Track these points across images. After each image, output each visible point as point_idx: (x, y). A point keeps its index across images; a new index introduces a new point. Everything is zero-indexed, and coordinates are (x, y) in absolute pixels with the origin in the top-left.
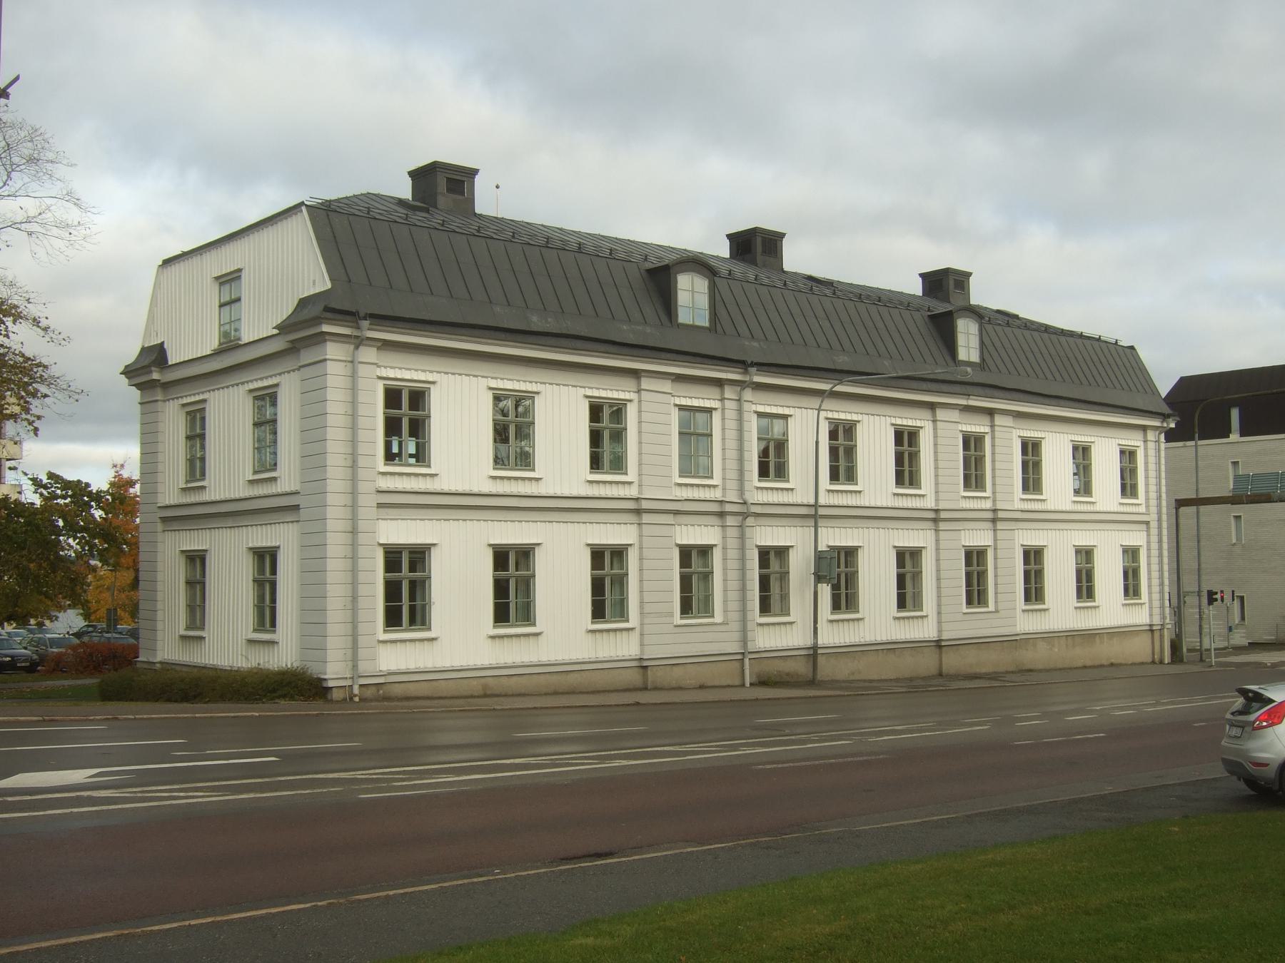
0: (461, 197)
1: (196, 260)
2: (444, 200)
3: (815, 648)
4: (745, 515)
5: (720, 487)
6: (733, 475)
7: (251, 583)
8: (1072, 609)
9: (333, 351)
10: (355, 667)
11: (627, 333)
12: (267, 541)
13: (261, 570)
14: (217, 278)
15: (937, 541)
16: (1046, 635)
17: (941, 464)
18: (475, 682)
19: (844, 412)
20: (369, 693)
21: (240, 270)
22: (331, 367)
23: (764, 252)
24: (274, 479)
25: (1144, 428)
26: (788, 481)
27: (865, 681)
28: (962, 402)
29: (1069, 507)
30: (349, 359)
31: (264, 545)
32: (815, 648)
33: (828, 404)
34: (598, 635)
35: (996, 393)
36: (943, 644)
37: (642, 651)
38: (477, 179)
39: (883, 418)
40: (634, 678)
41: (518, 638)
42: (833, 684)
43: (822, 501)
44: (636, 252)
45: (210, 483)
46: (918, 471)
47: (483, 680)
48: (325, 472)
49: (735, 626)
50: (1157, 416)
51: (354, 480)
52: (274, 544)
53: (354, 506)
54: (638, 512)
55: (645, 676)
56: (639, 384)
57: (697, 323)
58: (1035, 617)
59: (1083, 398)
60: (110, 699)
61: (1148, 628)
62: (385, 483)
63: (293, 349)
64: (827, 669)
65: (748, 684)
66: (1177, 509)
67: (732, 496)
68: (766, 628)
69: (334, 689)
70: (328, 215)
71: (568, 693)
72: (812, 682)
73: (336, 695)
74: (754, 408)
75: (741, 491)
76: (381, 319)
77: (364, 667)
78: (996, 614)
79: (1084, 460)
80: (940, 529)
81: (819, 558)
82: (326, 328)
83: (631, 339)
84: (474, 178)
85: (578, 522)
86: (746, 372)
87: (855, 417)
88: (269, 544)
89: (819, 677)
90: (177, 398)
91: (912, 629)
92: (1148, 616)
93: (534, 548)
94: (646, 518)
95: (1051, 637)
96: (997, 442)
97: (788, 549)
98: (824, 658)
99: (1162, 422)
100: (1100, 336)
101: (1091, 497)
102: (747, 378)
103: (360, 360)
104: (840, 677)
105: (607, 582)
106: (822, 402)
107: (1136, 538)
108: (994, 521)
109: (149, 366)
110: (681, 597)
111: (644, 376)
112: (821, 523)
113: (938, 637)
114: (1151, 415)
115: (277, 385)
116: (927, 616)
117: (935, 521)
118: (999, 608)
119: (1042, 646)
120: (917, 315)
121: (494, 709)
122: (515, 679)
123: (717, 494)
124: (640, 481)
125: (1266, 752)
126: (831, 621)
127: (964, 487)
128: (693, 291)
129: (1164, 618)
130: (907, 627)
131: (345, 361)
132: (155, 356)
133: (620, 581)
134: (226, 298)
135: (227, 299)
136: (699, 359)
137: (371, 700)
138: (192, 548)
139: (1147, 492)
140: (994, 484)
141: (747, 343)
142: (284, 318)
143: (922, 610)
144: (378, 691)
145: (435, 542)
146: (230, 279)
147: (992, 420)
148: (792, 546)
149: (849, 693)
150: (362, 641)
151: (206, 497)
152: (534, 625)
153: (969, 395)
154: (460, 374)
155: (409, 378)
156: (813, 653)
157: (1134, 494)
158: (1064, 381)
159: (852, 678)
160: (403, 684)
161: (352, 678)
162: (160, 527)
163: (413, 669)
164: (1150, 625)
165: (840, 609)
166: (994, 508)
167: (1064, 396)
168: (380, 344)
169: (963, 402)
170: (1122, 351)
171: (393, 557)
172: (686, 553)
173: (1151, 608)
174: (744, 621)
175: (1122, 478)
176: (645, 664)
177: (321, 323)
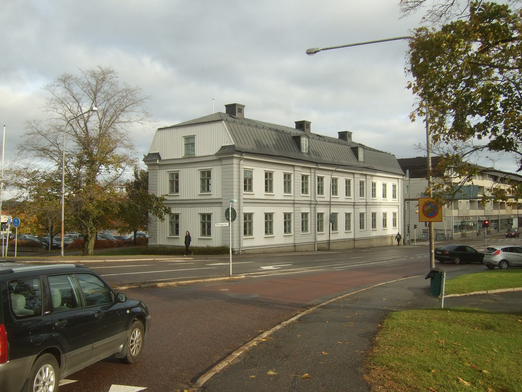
3: (329, 240)
4: (316, 204)
8: (344, 232)
9: (235, 161)
10: (240, 245)
12: (207, 211)
16: (301, 244)
18: (262, 250)
25: (398, 179)
26: (323, 195)
29: (391, 201)
32: (329, 240)
36: (356, 239)
37: (294, 241)
40: (292, 248)
42: (332, 250)
43: (331, 201)
49: (313, 235)
52: (251, 212)
55: (295, 248)
56: (294, 169)
64: (333, 246)
66: (405, 202)
67: (313, 199)
72: (329, 250)
75: (315, 198)
82: (235, 155)
86: (317, 165)
89: (330, 249)
94: (296, 205)
101: (323, 195)
102: (317, 167)
107: (396, 210)
112: (331, 206)
119: (375, 240)
123: (309, 199)
139: (398, 197)
140: (366, 195)
151: (180, 198)
156: (329, 242)
173: (399, 229)
174: (239, 237)
175: (346, 190)
176: (296, 245)
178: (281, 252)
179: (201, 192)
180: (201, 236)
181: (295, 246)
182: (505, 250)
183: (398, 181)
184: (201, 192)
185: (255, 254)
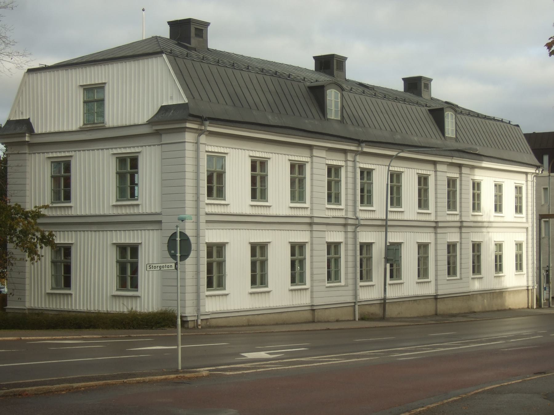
3: (385, 299)
4: (357, 226)
7: (115, 263)
8: (514, 275)
9: (189, 137)
17: (439, 196)
18: (244, 318)
23: (337, 69)
24: (138, 205)
29: (249, 211)
30: (195, 142)
32: (385, 299)
36: (439, 297)
37: (312, 301)
38: (432, 83)
39: (413, 170)
40: (308, 316)
41: (215, 297)
44: (177, 50)
47: (248, 317)
48: (185, 203)
49: (351, 287)
50: (534, 167)
55: (313, 315)
56: (312, 153)
58: (394, 287)
59: (348, 136)
62: (209, 210)
64: (391, 311)
65: (357, 319)
67: (350, 215)
69: (189, 322)
70: (175, 59)
71: (281, 324)
72: (383, 318)
75: (355, 212)
76: (215, 120)
77: (202, 310)
80: (438, 232)
81: (388, 249)
84: (207, 28)
85: (253, 230)
86: (359, 145)
87: (401, 170)
92: (526, 282)
93: (267, 244)
94: (315, 227)
97: (340, 244)
100: (502, 119)
102: (360, 149)
106: (391, 162)
113: (435, 293)
114: (531, 166)
116: (430, 282)
118: (463, 277)
120: (423, 109)
121: (273, 332)
122: (260, 316)
127: (418, 207)
130: (424, 286)
131: (193, 143)
136: (340, 139)
139: (527, 210)
141: (357, 129)
143: (428, 278)
144: (207, 323)
145: (270, 241)
147: (461, 170)
149: (413, 324)
153: (453, 157)
156: (384, 303)
158: (514, 151)
159: (398, 316)
163: (226, 310)
166: (461, 220)
167: (494, 156)
168: (327, 149)
169: (449, 160)
170: (513, 128)
173: (528, 277)
176: (315, 308)
178: (284, 323)
179: (117, 200)
180: (117, 290)
181: (313, 310)
184: (117, 200)
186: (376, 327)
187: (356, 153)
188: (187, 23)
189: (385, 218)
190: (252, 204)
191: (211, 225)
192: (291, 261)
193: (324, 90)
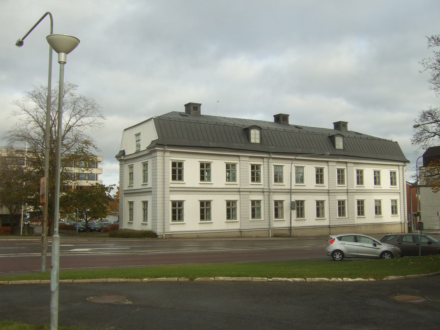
0: (197, 111)
1: (131, 130)
2: (192, 112)
3: (291, 227)
4: (270, 192)
5: (263, 185)
6: (267, 181)
7: (142, 210)
9: (159, 154)
10: (164, 230)
11: (236, 146)
13: (145, 207)
14: (135, 135)
15: (329, 198)
18: (195, 234)
19: (300, 164)
20: (167, 236)
21: (140, 133)
22: (158, 158)
23: (283, 120)
24: (147, 184)
26: (283, 183)
27: (304, 236)
28: (336, 160)
30: (163, 156)
31: (145, 200)
32: (291, 227)
33: (294, 162)
34: (228, 223)
35: (347, 157)
36: (331, 226)
38: (348, 124)
40: (238, 234)
41: (206, 224)
42: (296, 237)
45: (134, 185)
46: (323, 179)
49: (267, 221)
51: (164, 185)
52: (147, 200)
53: (164, 191)
54: (239, 192)
56: (328, 164)
57: (256, 142)
59: (376, 158)
60: (111, 237)
61: (400, 223)
63: (150, 153)
64: (294, 233)
68: (276, 222)
72: (290, 236)
73: (159, 237)
74: (273, 164)
75: (269, 186)
77: (166, 230)
78: (348, 218)
79: (378, 175)
82: (157, 148)
83: (237, 147)
86: (270, 155)
88: (146, 200)
90: (127, 164)
91: (396, 219)
94: (241, 193)
95: (366, 225)
96: (348, 171)
98: (294, 230)
99: (404, 164)
103: (165, 156)
104: (299, 235)
105: (256, 209)
106: (292, 162)
107: (396, 197)
108: (347, 193)
109: (121, 156)
110: (252, 214)
111: (241, 157)
112: (292, 194)
115: (147, 161)
117: (328, 193)
124: (240, 184)
125: (329, 249)
126: (296, 220)
128: (255, 134)
129: (405, 220)
132: (123, 153)
133: (235, 209)
134: (137, 140)
135: (138, 140)
137: (168, 238)
138: (130, 201)
142: (149, 145)
144: (170, 236)
146: (138, 135)
148: (284, 200)
150: (166, 224)
151: (133, 188)
152: (211, 220)
154: (189, 158)
155: (178, 159)
156: (290, 229)
157: (395, 184)
159: (302, 235)
160: (176, 235)
161: (163, 233)
162: (124, 195)
164: (401, 222)
165: (299, 217)
168: (170, 152)
169: (337, 160)
171: (174, 204)
172: (253, 202)
174: (269, 220)
176: (241, 231)
177: (155, 147)
178: (221, 237)
181: (241, 232)
182: (340, 239)
183: (399, 168)
185: (186, 238)
186: (269, 240)
187: (269, 158)
188: (340, 122)
189: (290, 188)
190: (251, 184)
191: (171, 193)
192: (375, 206)
193: (334, 137)
